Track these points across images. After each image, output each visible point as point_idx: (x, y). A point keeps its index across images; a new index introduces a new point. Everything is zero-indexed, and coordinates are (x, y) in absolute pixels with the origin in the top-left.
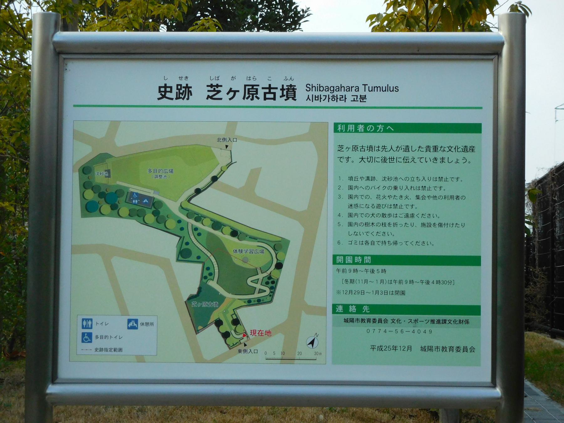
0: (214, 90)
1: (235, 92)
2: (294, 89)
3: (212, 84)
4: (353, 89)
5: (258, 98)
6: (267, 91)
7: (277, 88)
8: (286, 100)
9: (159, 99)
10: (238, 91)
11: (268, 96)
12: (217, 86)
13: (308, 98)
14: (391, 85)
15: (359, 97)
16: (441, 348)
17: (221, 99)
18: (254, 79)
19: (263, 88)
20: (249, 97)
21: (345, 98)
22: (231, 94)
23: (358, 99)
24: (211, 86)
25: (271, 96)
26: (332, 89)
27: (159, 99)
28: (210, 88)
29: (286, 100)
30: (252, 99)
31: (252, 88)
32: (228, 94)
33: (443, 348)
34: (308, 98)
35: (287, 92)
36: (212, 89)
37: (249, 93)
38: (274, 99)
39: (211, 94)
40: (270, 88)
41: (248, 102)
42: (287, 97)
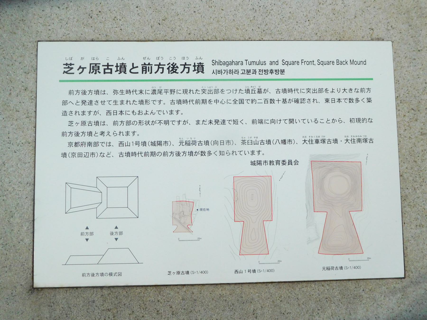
0: (69, 67)
1: (83, 68)
2: (125, 66)
3: (67, 63)
4: (240, 63)
5: (100, 73)
6: (106, 67)
7: (113, 66)
8: (119, 73)
9: (133, 64)
10: (86, 68)
11: (106, 71)
12: (71, 64)
13: (213, 72)
14: (261, 60)
15: (246, 71)
16: (269, 162)
17: (73, 73)
18: (97, 59)
19: (103, 66)
20: (93, 71)
21: (238, 72)
22: (81, 70)
23: (246, 73)
24: (67, 64)
25: (109, 71)
26: (227, 63)
27: (133, 64)
28: (65, 66)
29: (119, 73)
30: (96, 73)
31: (96, 66)
32: (78, 70)
33: (270, 162)
34: (213, 72)
35: (198, 68)
36: (67, 67)
37: (93, 69)
38: (111, 73)
39: (66, 70)
40: (108, 65)
41: (93, 76)
42: (198, 71)
